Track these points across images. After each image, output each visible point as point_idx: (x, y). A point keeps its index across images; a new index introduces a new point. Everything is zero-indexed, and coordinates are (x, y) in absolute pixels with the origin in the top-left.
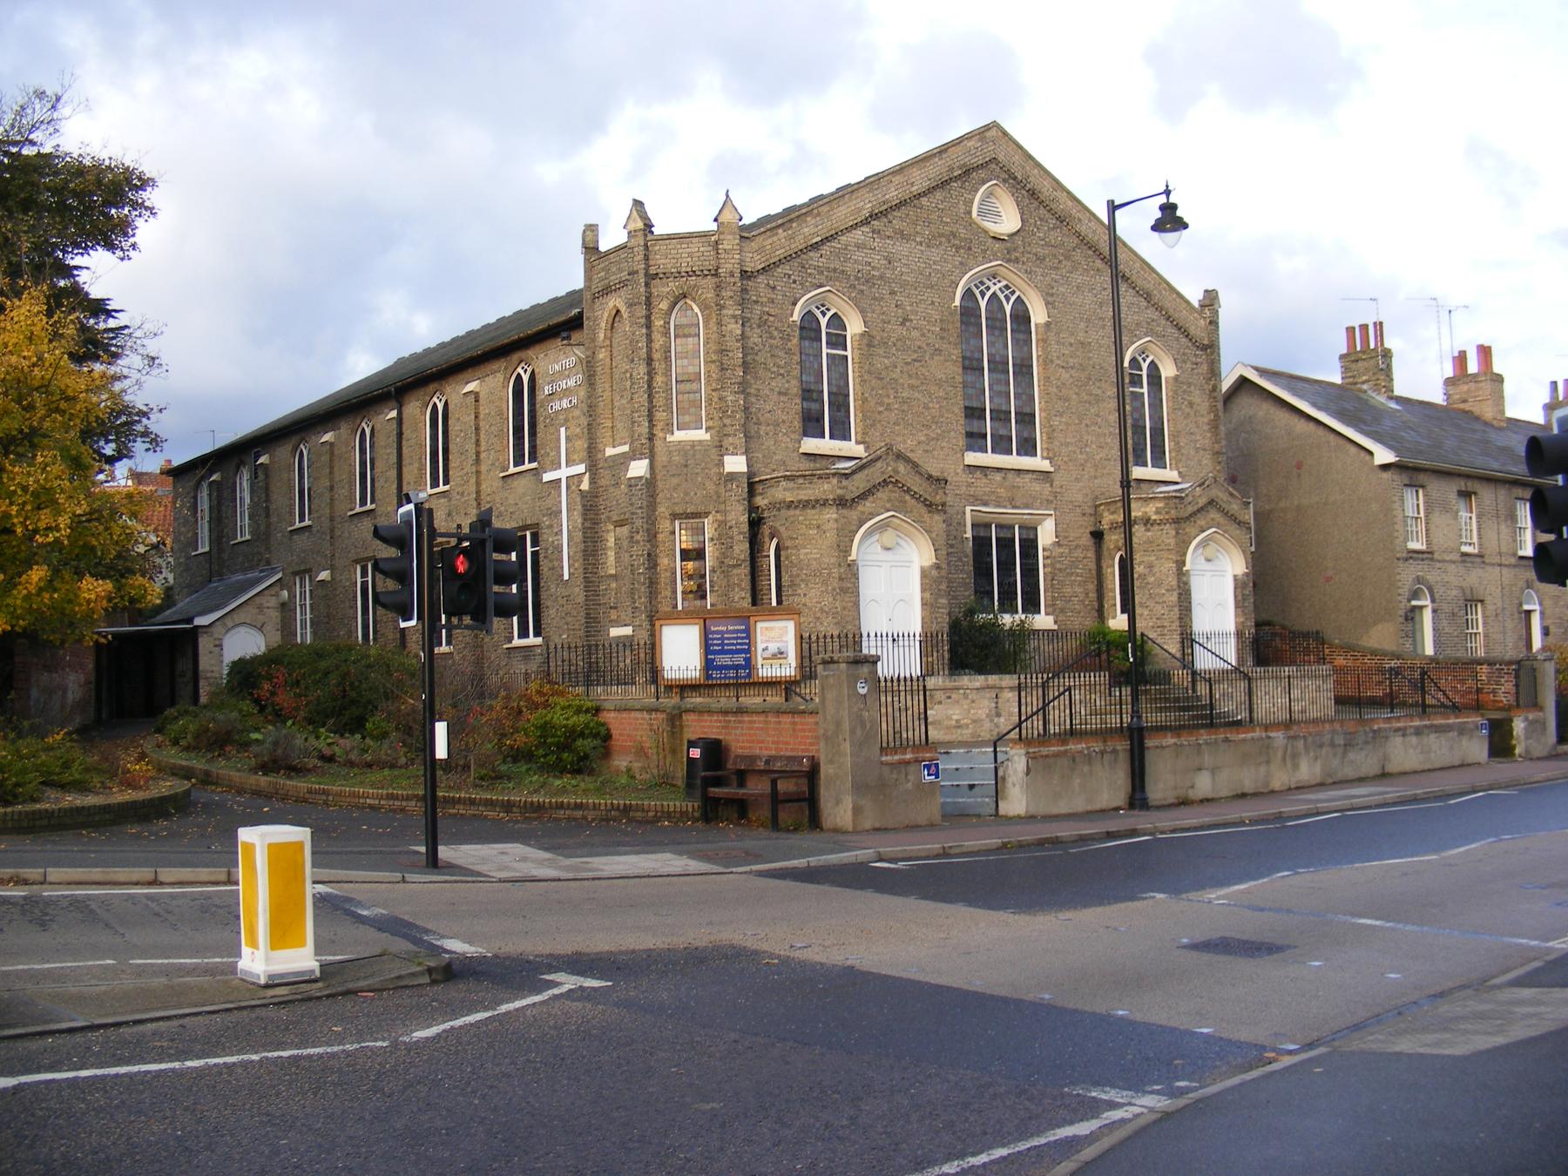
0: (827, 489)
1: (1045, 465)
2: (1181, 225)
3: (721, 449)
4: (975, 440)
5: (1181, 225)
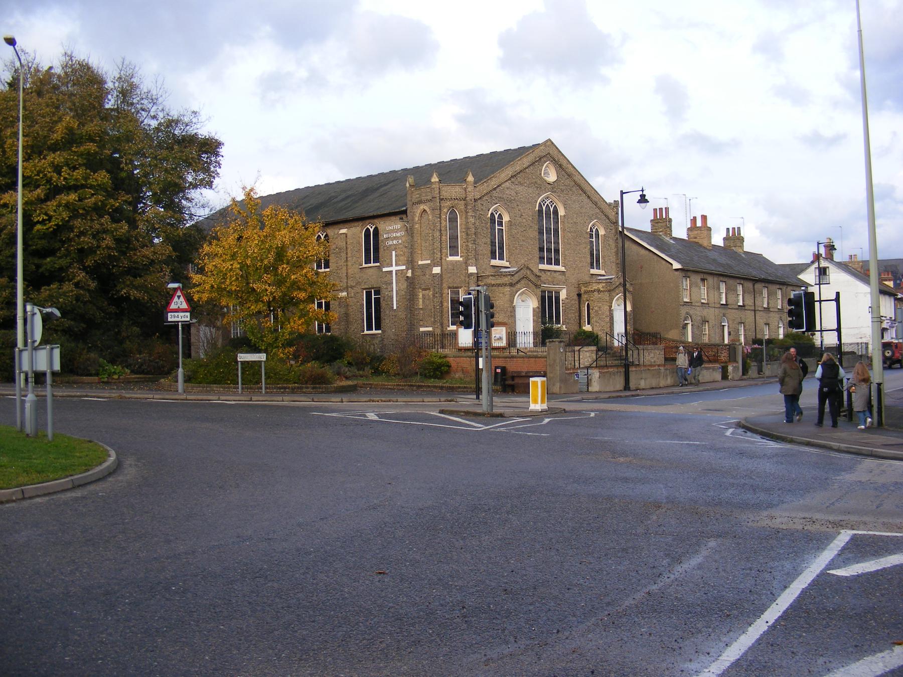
0: (506, 280)
1: (563, 269)
2: (647, 201)
3: (467, 264)
4: (541, 259)
5: (647, 201)
